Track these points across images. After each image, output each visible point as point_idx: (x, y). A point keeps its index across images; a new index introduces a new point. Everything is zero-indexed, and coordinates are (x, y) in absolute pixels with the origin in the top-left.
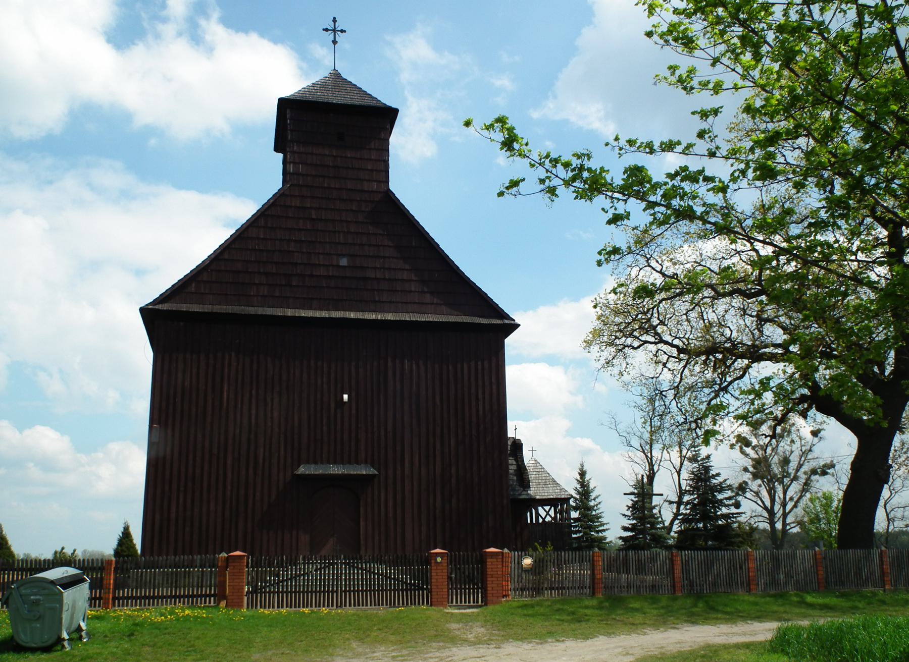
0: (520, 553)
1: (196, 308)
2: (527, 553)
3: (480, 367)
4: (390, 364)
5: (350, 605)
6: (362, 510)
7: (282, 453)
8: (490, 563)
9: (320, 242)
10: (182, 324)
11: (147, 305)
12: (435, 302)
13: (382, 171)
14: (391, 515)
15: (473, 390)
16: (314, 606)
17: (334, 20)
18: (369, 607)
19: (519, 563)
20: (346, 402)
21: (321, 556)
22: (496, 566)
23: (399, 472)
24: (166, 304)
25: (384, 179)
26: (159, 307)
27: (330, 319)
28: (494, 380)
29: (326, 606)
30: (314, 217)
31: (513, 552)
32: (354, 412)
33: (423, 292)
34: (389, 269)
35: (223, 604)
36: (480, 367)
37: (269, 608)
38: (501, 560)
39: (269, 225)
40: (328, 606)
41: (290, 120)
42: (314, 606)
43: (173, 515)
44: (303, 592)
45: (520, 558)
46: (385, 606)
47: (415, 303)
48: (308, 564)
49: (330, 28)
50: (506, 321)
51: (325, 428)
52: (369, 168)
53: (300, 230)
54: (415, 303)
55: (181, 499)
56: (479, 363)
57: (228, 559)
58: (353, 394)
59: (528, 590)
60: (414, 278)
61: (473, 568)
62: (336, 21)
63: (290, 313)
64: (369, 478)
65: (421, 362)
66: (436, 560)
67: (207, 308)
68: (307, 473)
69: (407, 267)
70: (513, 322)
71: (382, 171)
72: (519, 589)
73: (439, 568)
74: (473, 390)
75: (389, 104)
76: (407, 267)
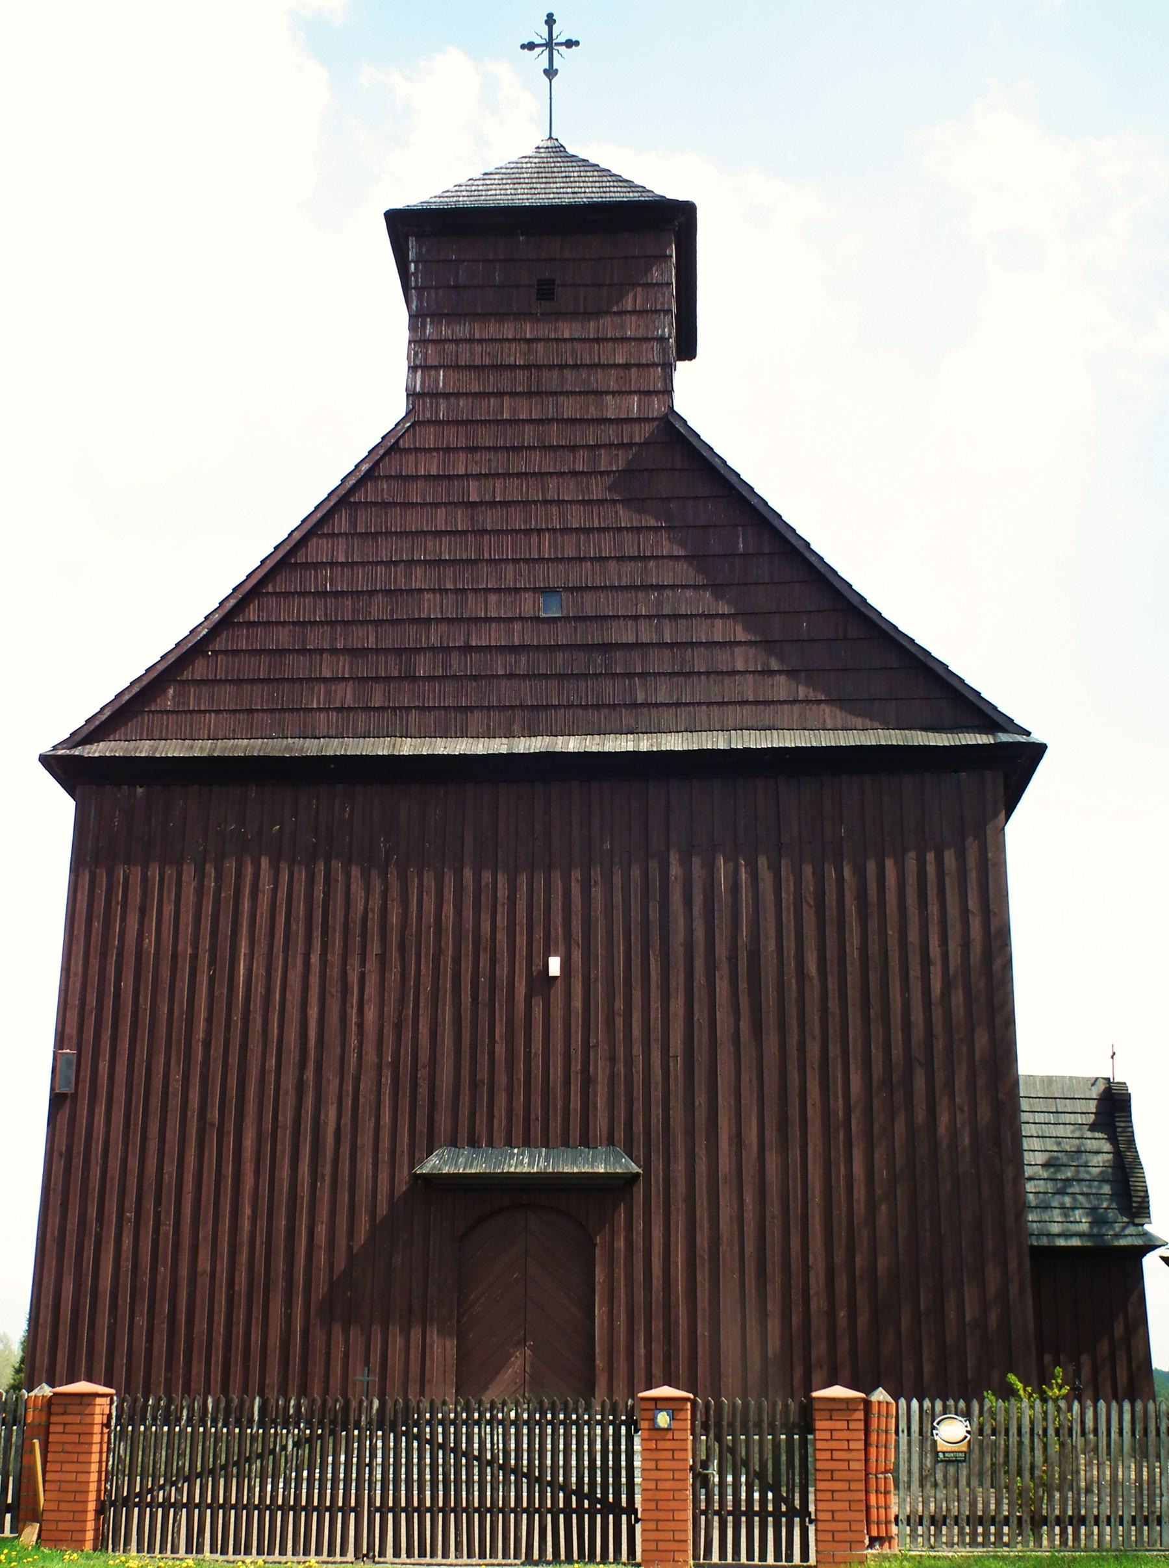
0: (927, 1404)
1: (172, 749)
2: (951, 1403)
3: (931, 869)
4: (675, 870)
5: (397, 1554)
6: (600, 1276)
7: (386, 1118)
8: (827, 1435)
9: (490, 561)
10: (140, 790)
11: (55, 748)
12: (801, 697)
13: (655, 365)
14: (680, 1286)
15: (913, 936)
16: (207, 1548)
17: (550, 21)
18: (452, 1559)
19: (926, 1436)
20: (555, 978)
21: (432, 1403)
22: (844, 1445)
23: (702, 1167)
24: (101, 744)
25: (660, 386)
26: (96, 750)
27: (511, 757)
28: (973, 904)
29: (254, 1551)
30: (474, 498)
31: (902, 1402)
32: (577, 1003)
33: (770, 673)
34: (675, 617)
35: (31, 1533)
36: (931, 869)
37: (306, 1552)
38: (861, 1425)
39: (361, 529)
40: (318, 1552)
41: (416, 263)
42: (207, 1548)
43: (106, 1283)
44: (482, 1510)
45: (928, 1422)
46: (325, 1557)
47: (747, 702)
48: (566, 1424)
49: (538, 41)
50: (1004, 738)
51: (500, 1049)
52: (620, 360)
53: (437, 534)
54: (747, 702)
55: (127, 1243)
56: (930, 857)
57: (50, 1402)
58: (577, 955)
59: (1097, 1523)
60: (741, 636)
61: (776, 1444)
62: (555, 21)
63: (407, 747)
64: (625, 1183)
65: (762, 862)
66: (653, 1420)
67: (200, 748)
68: (445, 1171)
69: (723, 608)
70: (1022, 739)
71: (655, 365)
72: (926, 1522)
73: (662, 1445)
74: (913, 936)
75: (671, 195)
76: (723, 608)
